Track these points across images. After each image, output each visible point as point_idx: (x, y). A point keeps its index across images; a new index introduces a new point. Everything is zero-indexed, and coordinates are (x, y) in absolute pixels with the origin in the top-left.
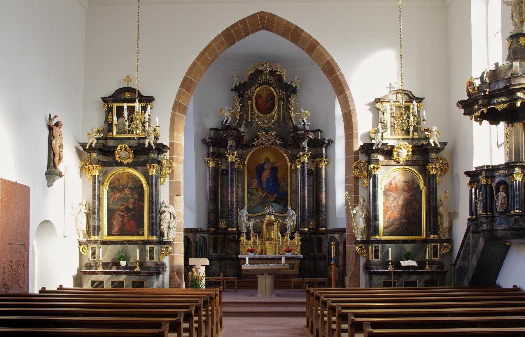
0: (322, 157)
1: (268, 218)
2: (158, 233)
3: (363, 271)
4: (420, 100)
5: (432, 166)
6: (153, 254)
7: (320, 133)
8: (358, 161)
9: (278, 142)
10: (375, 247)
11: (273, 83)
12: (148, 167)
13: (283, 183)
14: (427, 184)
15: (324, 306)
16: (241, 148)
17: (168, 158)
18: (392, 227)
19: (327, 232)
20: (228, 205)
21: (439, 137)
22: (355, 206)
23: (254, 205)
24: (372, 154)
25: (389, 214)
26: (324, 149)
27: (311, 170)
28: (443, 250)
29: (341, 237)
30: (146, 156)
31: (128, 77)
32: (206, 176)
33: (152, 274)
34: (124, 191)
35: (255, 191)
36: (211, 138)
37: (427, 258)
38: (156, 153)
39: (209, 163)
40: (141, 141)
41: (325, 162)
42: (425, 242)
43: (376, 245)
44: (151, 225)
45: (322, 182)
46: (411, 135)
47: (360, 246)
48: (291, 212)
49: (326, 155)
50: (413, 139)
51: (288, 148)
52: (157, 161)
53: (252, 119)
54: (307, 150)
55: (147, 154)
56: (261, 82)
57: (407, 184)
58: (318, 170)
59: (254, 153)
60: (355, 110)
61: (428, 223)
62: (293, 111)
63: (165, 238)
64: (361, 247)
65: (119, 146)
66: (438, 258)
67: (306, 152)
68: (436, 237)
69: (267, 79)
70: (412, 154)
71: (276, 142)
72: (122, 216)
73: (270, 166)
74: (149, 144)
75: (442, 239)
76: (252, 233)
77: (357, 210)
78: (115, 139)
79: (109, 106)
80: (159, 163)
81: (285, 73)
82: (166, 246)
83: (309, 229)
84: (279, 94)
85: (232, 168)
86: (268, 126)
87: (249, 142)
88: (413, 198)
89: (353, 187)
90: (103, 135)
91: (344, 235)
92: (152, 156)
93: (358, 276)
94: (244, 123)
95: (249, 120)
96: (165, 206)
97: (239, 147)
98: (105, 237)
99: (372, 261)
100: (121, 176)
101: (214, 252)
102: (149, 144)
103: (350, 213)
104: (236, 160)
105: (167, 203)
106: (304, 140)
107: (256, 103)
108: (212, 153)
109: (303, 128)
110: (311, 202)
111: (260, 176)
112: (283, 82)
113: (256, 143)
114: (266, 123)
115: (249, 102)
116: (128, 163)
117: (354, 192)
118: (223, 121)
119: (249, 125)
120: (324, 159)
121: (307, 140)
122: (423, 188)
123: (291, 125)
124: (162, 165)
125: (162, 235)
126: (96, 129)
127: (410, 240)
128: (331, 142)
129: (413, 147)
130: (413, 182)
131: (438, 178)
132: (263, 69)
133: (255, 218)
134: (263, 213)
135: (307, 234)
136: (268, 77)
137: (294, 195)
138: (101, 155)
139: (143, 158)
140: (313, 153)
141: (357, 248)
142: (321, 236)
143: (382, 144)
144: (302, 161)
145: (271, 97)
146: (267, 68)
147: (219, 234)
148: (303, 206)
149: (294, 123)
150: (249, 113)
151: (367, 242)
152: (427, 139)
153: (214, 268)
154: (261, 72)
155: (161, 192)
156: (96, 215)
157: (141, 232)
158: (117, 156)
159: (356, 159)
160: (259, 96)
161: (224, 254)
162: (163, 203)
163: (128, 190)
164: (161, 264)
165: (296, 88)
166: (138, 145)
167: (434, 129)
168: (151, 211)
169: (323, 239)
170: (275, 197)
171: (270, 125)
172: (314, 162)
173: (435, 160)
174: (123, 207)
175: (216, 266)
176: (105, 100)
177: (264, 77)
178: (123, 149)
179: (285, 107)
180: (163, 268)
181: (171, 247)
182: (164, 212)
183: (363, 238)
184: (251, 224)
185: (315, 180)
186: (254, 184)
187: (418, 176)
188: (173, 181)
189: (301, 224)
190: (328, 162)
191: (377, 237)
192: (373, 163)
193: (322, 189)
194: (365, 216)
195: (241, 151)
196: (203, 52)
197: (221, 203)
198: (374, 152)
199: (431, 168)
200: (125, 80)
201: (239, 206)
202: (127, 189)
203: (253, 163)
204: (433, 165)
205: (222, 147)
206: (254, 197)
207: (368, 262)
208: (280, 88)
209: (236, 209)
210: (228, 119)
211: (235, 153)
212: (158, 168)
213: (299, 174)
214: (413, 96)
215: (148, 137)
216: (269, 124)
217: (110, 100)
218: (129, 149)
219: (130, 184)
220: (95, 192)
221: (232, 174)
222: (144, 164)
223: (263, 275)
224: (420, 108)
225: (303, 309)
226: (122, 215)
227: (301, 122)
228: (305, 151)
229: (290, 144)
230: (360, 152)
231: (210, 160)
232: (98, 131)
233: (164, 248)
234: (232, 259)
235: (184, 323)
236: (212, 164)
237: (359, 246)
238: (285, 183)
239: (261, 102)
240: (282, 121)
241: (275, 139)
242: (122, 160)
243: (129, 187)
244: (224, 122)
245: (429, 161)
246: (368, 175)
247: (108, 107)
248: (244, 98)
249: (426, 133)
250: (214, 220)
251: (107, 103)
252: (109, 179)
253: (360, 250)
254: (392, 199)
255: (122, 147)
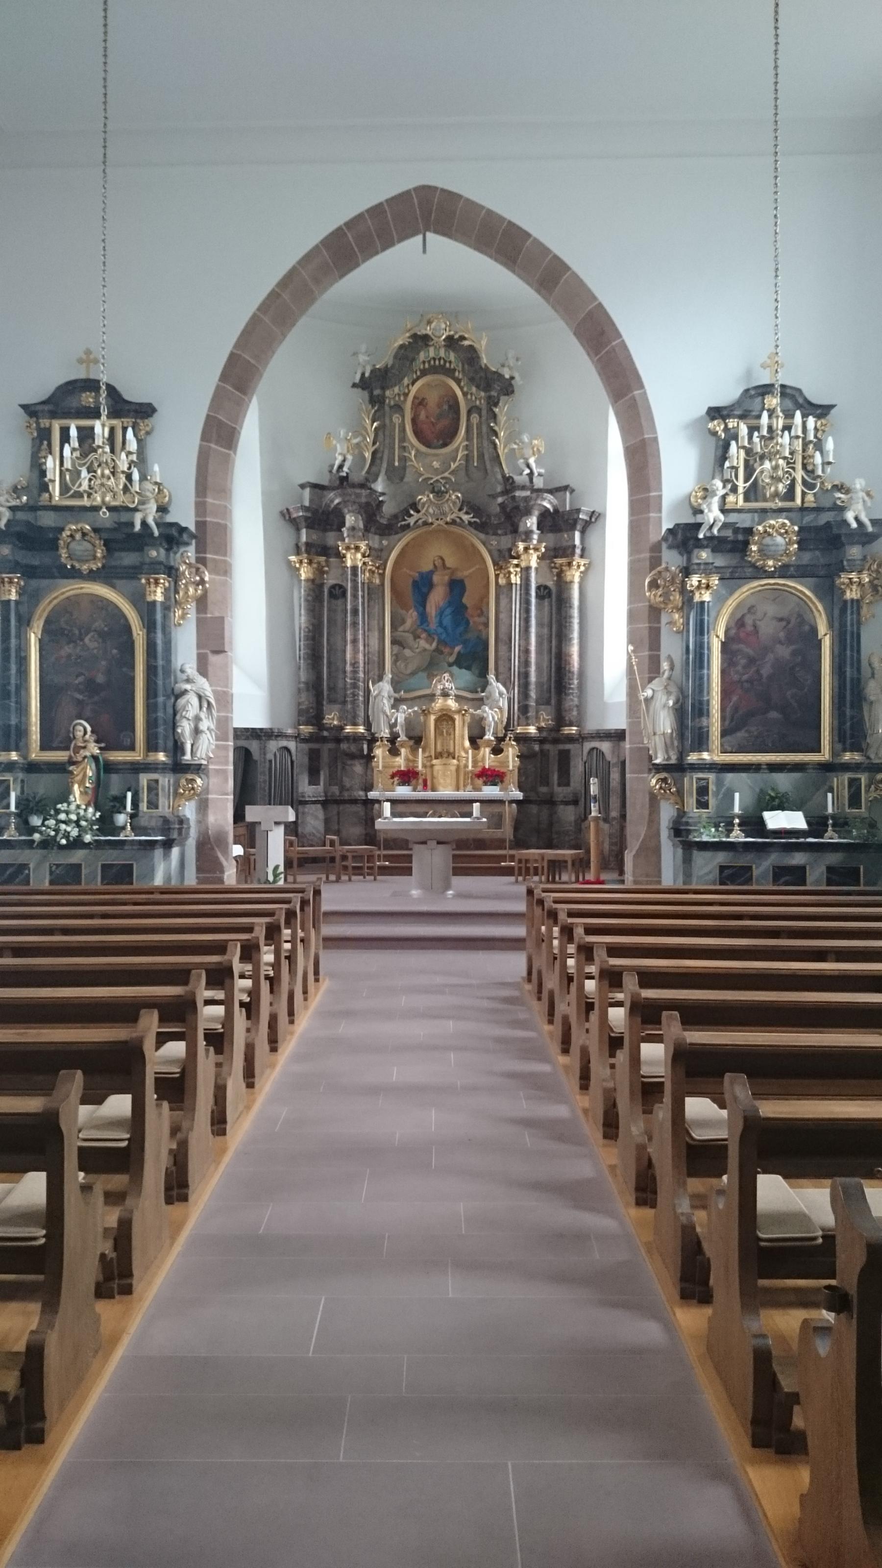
0: (573, 554)
1: (439, 703)
2: (170, 744)
3: (669, 837)
4: (822, 411)
5: (850, 579)
6: (157, 795)
7: (568, 494)
8: (659, 569)
9: (466, 518)
10: (699, 779)
11: (455, 370)
12: (143, 581)
13: (476, 619)
14: (836, 624)
15: (566, 938)
16: (376, 534)
17: (193, 561)
18: (743, 731)
19: (580, 738)
20: (345, 672)
21: (869, 504)
22: (650, 680)
23: (409, 671)
24: (696, 551)
25: (735, 698)
26: (577, 535)
27: (546, 587)
28: (876, 789)
29: (617, 750)
30: (137, 554)
31: (88, 352)
32: (292, 602)
33: (152, 844)
34: (82, 640)
35: (409, 637)
36: (304, 508)
37: (830, 810)
38: (163, 547)
39: (298, 570)
40: (124, 517)
41: (579, 566)
42: (827, 768)
43: (701, 775)
44: (151, 724)
45: (571, 617)
46: (798, 501)
47: (662, 777)
48: (496, 687)
49: (583, 550)
50: (803, 509)
51: (491, 532)
52: (165, 566)
53: (404, 459)
54: (535, 537)
55: (140, 549)
56: (427, 365)
57: (784, 623)
58: (563, 585)
59: (407, 545)
60: (656, 440)
61: (836, 723)
62: (503, 440)
63: (188, 757)
64: (664, 780)
65: (67, 528)
66: (863, 810)
67: (535, 542)
68: (857, 757)
69: (440, 359)
70: (800, 549)
71: (461, 519)
72: (79, 702)
73: (447, 578)
74: (144, 523)
75: (872, 764)
76: (403, 737)
77: (653, 690)
78: (57, 509)
79: (42, 426)
80: (172, 572)
81: (484, 343)
82: (190, 776)
83: (539, 729)
84: (469, 397)
85: (354, 581)
86: (442, 478)
87: (395, 517)
88: (799, 659)
89: (646, 633)
90: (28, 500)
91: (622, 744)
92: (154, 553)
93: (657, 851)
94: (383, 471)
95: (397, 464)
96: (185, 678)
97: (373, 529)
98: (34, 756)
99: (691, 815)
100: (73, 602)
101: (310, 783)
102: (144, 523)
103: (637, 697)
104: (364, 563)
105: (191, 668)
106: (528, 513)
107: (414, 421)
108: (307, 544)
109: (528, 484)
110: (545, 664)
111: (422, 601)
112: (481, 367)
113: (411, 521)
114: (437, 471)
115: (396, 419)
116: (91, 571)
117: (647, 646)
118: (332, 466)
119: (396, 475)
120: (577, 559)
121: (536, 513)
122: (825, 635)
123: (499, 477)
124: (177, 576)
125: (177, 748)
126: (8, 483)
127: (788, 764)
128: (596, 518)
129: (801, 529)
130: (798, 620)
131: (864, 610)
132: (430, 333)
133: (409, 703)
134: (427, 692)
135: (535, 741)
136: (442, 353)
137: (503, 648)
138: (22, 548)
139: (129, 559)
140: (552, 545)
141: (654, 781)
142: (568, 746)
143: (720, 524)
144: (523, 564)
145: (451, 403)
146: (440, 329)
147: (324, 740)
148: (525, 676)
149: (506, 471)
150: (397, 446)
151: (679, 768)
152: (842, 509)
153: (312, 822)
154: (425, 340)
155: (176, 644)
156: (13, 699)
157: (128, 742)
158: (63, 553)
159: (655, 562)
160: (420, 403)
161: (335, 790)
162: (182, 671)
163: (93, 637)
164: (176, 819)
165: (513, 382)
166: (116, 526)
167: (859, 484)
168: (151, 692)
169: (572, 752)
170: (459, 653)
171: (446, 474)
172: (553, 568)
173: (858, 562)
174: (81, 679)
175: (316, 818)
176: (30, 410)
177: (432, 353)
178: (78, 536)
179: (484, 429)
180: (180, 830)
181: (200, 777)
182: (186, 692)
183: (669, 758)
184: (401, 717)
185: (554, 612)
186: (409, 623)
187: (814, 603)
188: (206, 618)
189: (519, 717)
190: (588, 567)
191: (705, 756)
192: (696, 574)
193: (572, 632)
194: (675, 704)
195: (376, 541)
196: (277, 290)
197: (329, 667)
198: (699, 545)
199: (848, 585)
200: (80, 361)
201: (371, 674)
202: (89, 636)
203: (405, 569)
204: (853, 575)
205: (331, 530)
206: (407, 652)
207: (683, 817)
208: (472, 380)
209: (364, 682)
210: (344, 461)
211: (363, 546)
212: (167, 584)
213: (516, 595)
214: (806, 399)
215: (140, 507)
216: (443, 473)
217: (43, 411)
218: (92, 534)
219: (97, 624)
220: (9, 643)
221: (355, 596)
222: (133, 573)
223: (424, 843)
224: (824, 431)
225: (519, 931)
226: (78, 700)
227: (523, 466)
228: (531, 539)
229: (495, 522)
230: (664, 546)
231: (301, 562)
232: (15, 489)
233: (183, 782)
234: (354, 801)
235: (206, 989)
236: (305, 573)
237: (658, 776)
238: (482, 619)
239: (427, 417)
240: (475, 464)
241: (460, 510)
242: (77, 565)
243: (95, 631)
244: (336, 467)
245: (843, 566)
246: (683, 603)
247: (39, 429)
248: (383, 407)
249: (838, 495)
250: (312, 708)
251: (35, 419)
252: (44, 610)
253: (661, 788)
254: (743, 662)
255: (76, 531)
